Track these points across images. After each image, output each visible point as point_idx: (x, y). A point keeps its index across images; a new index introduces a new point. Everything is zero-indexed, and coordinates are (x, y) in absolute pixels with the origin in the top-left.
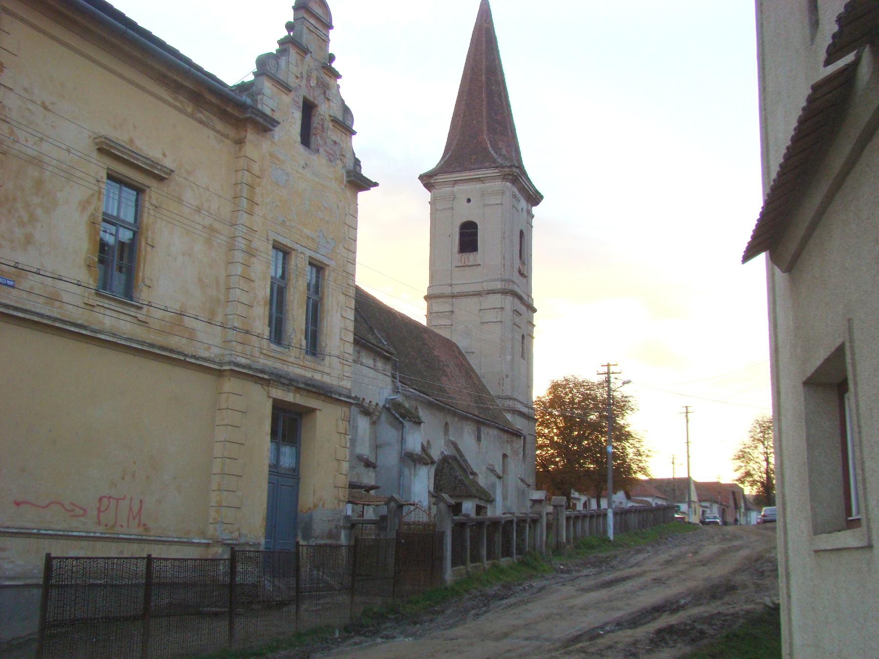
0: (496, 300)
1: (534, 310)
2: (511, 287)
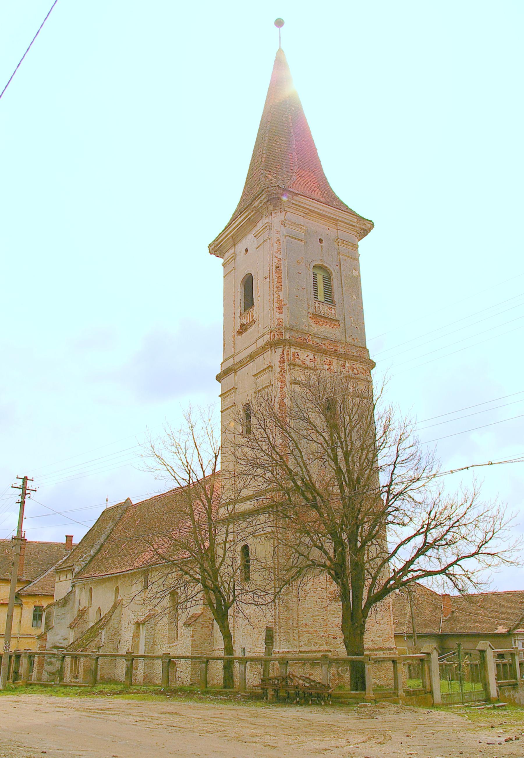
0: (260, 363)
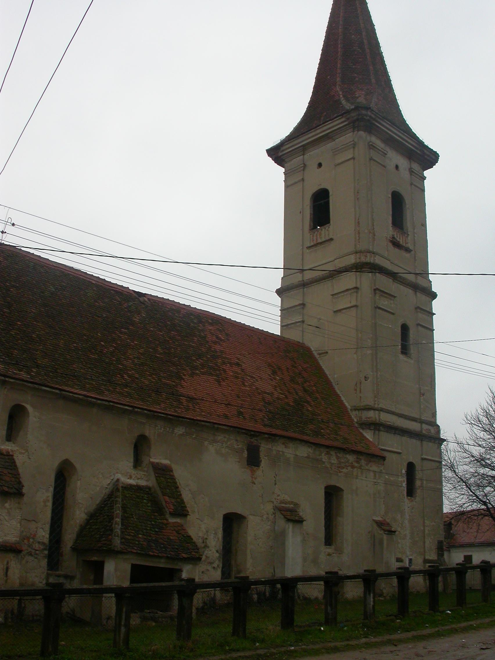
0: (349, 280)
1: (434, 296)
2: (369, 259)
